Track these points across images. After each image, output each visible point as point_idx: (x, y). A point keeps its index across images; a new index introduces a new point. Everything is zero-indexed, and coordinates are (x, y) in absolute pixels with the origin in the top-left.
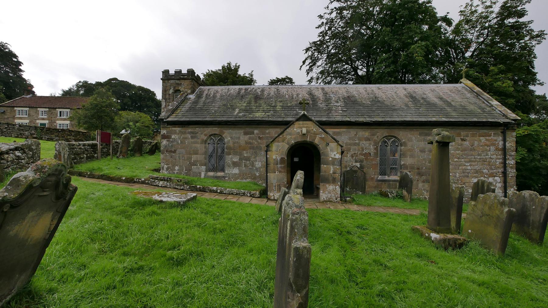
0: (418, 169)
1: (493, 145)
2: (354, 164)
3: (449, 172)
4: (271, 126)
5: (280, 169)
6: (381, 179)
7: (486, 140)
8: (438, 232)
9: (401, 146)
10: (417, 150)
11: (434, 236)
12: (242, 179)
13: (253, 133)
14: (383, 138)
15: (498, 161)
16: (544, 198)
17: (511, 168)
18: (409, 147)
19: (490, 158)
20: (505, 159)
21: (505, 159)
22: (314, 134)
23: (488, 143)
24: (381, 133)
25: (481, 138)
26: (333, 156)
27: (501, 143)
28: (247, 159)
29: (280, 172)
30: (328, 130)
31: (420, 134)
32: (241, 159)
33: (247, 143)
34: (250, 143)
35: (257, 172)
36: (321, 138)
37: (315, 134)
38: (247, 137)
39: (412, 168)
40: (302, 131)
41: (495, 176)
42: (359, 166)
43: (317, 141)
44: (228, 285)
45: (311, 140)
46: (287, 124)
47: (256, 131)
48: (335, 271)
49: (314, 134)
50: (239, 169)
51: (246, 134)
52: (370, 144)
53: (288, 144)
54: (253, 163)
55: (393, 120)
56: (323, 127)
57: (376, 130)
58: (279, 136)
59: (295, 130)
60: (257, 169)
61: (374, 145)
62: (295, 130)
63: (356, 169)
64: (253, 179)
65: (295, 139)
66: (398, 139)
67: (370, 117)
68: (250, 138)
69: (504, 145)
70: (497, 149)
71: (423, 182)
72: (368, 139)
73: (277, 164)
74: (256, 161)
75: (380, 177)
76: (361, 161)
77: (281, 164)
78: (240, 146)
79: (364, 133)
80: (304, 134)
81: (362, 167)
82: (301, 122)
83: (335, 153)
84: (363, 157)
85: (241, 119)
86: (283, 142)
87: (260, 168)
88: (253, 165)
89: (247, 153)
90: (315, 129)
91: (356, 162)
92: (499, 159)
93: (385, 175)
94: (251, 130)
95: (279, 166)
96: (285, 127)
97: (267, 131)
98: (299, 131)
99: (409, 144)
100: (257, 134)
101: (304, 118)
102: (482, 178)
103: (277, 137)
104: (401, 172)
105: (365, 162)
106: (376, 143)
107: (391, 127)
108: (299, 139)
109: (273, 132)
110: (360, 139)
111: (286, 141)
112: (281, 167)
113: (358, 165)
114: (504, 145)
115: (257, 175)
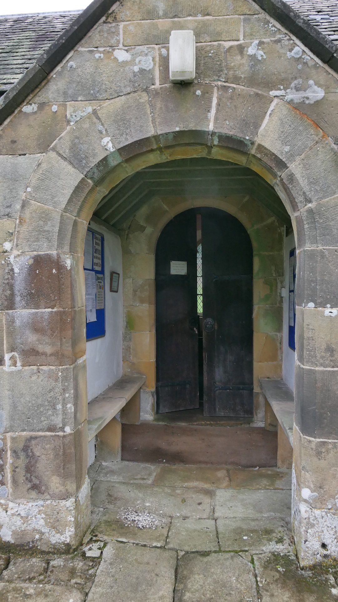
5: (32, 338)
16: (150, 467)
22: (252, 81)
29: (30, 355)
36: (299, 108)
37: (262, 82)
40: (165, 61)
43: (270, 133)
45: (229, 128)
48: (279, 41)
49: (252, 81)
53: (76, 158)
59: (121, 55)
62: (121, 55)
65: (121, 120)
73: (11, 306)
77: (33, 299)
80: (183, 85)
86: (44, 147)
95: (23, 313)
98: (147, 61)
111: (64, 140)
112: (36, 327)
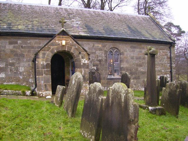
0: (130, 70)
1: (166, 55)
2: (93, 68)
3: (155, 72)
4: (32, 38)
6: (110, 78)
7: (163, 52)
8: (151, 106)
9: (121, 55)
10: (129, 58)
11: (150, 108)
12: (8, 82)
13: (17, 43)
14: (110, 48)
15: (168, 64)
17: (174, 69)
18: (125, 55)
19: (165, 63)
20: (171, 64)
21: (171, 64)
23: (164, 54)
24: (109, 45)
25: (161, 51)
26: (83, 62)
27: (169, 54)
28: (12, 64)
30: (80, 42)
31: (131, 47)
32: (7, 65)
33: (12, 51)
34: (14, 51)
35: (21, 75)
38: (11, 47)
39: (127, 70)
40: (62, 43)
41: (167, 74)
42: (96, 69)
43: (72, 51)
44: (144, 120)
46: (51, 36)
47: (19, 42)
50: (5, 74)
51: (10, 43)
52: (102, 53)
54: (17, 68)
55: (116, 37)
56: (75, 40)
57: (107, 43)
58: (45, 46)
60: (21, 73)
61: (104, 54)
63: (94, 71)
64: (18, 81)
65: (57, 49)
66: (119, 50)
67: (134, 36)
68: (14, 47)
69: (171, 55)
70: (168, 58)
71: (133, 79)
72: (100, 50)
74: (20, 66)
75: (109, 77)
76: (97, 65)
78: (6, 54)
79: (98, 45)
81: (97, 70)
82: (61, 36)
83: (85, 59)
84: (98, 62)
85: (5, 31)
87: (23, 72)
88: (17, 70)
89: (12, 60)
90: (71, 41)
91: (94, 66)
92: (169, 64)
93: (112, 75)
94: (15, 40)
96: (50, 39)
97: (29, 42)
99: (126, 53)
100: (21, 44)
101: (64, 33)
102: (162, 75)
103: (43, 47)
104: (121, 73)
105: (99, 66)
106: (106, 52)
107: (115, 41)
108: (60, 49)
109: (43, 42)
110: (96, 49)
113: (95, 68)
114: (171, 55)
115: (21, 78)
